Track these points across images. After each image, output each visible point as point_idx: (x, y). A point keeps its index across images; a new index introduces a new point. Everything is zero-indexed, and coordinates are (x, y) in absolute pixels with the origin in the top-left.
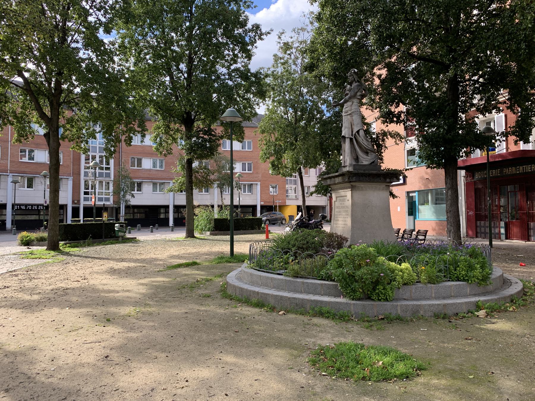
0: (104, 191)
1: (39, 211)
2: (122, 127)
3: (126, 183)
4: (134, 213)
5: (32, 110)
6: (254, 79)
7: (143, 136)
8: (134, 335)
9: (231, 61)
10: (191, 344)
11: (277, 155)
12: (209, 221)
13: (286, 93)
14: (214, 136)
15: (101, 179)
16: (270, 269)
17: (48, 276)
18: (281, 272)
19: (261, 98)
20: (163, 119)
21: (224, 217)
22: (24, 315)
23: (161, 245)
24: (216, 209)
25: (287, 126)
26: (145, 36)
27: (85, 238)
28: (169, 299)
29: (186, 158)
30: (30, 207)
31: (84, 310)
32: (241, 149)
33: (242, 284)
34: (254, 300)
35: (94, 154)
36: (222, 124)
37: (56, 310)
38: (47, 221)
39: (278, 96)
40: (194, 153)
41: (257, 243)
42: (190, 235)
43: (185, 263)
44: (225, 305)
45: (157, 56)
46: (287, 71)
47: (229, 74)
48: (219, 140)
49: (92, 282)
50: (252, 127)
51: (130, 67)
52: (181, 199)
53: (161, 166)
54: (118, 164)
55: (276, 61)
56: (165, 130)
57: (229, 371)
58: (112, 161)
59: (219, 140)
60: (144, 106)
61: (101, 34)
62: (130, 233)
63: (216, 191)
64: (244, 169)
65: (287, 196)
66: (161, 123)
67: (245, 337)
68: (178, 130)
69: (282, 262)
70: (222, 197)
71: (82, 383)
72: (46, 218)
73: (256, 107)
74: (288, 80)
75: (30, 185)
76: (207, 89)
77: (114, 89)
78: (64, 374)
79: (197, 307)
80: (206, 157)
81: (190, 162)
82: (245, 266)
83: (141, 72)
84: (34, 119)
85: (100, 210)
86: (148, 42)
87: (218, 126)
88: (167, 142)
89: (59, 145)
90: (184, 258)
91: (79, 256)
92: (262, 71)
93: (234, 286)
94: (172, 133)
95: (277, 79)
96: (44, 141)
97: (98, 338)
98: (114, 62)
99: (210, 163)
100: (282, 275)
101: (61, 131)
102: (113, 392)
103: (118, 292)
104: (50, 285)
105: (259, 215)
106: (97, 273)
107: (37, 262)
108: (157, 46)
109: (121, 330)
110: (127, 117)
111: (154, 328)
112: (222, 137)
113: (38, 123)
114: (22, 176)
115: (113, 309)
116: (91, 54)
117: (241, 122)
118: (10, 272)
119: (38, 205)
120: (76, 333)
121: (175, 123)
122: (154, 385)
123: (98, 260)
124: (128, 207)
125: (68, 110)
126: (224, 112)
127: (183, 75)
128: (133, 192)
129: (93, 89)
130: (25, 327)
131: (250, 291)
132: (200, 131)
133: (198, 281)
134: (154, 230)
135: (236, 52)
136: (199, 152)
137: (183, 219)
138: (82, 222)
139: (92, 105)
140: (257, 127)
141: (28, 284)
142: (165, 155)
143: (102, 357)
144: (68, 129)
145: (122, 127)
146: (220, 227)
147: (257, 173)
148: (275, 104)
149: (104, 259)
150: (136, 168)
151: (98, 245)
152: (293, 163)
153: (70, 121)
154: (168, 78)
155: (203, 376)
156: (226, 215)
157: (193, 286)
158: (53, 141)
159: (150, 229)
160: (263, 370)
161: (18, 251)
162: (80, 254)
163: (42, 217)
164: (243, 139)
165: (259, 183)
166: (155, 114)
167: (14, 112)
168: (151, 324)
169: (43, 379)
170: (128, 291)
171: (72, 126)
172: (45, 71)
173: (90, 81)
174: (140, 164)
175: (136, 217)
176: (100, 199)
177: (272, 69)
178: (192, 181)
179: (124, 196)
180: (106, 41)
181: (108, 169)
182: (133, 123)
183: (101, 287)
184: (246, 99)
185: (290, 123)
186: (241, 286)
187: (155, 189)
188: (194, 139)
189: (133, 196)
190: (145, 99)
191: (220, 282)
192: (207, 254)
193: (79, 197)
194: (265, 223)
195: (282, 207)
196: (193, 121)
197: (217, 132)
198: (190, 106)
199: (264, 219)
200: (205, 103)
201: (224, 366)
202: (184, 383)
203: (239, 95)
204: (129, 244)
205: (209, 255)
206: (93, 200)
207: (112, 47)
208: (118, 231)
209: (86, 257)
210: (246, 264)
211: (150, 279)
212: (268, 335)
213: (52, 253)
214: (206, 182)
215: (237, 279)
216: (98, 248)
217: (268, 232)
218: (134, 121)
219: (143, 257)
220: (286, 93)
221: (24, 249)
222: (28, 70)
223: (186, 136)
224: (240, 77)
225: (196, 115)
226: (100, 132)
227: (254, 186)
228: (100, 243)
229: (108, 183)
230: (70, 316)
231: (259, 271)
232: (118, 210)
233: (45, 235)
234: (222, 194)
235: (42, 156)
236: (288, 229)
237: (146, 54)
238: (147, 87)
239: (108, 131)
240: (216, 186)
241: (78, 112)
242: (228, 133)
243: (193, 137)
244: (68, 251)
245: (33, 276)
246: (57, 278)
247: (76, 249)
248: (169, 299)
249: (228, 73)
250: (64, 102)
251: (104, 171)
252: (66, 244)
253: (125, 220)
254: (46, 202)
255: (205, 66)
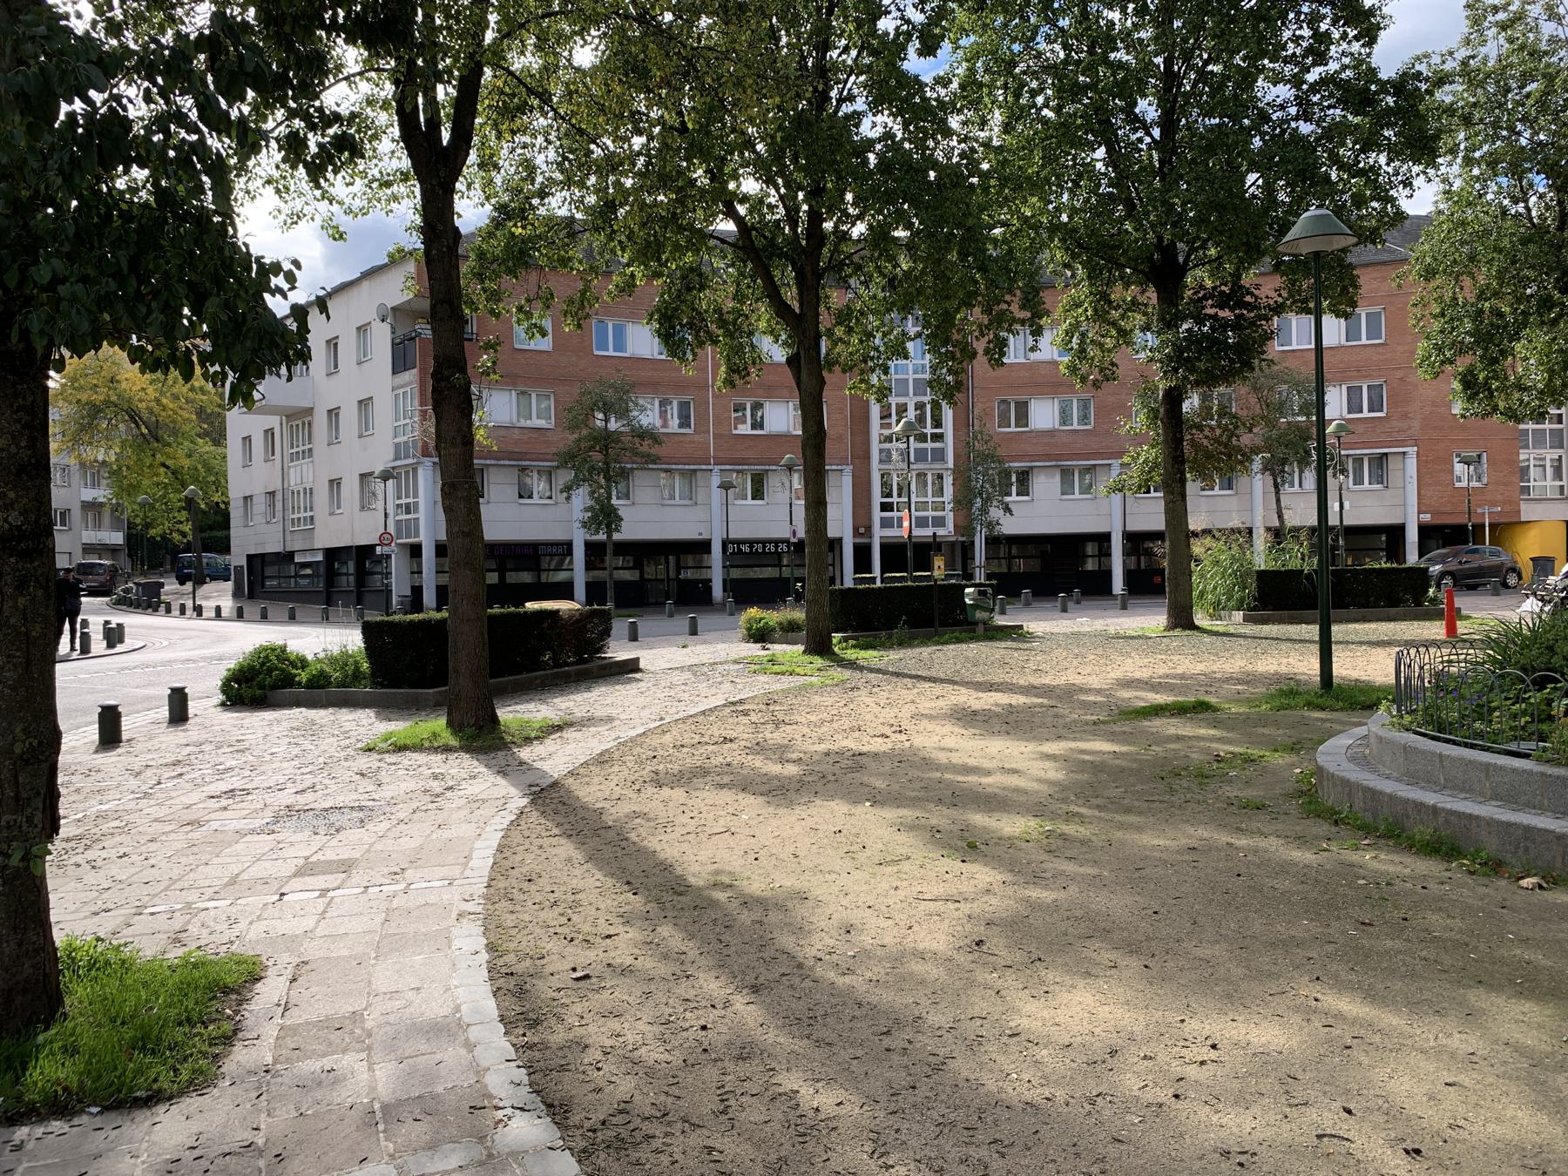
0: (930, 499)
1: (779, 555)
2: (977, 314)
3: (988, 473)
4: (1010, 558)
5: (757, 300)
6: (1390, 100)
7: (1037, 332)
8: (1047, 896)
9: (1304, 57)
10: (1217, 942)
11: (1486, 349)
12: (1242, 577)
13: (1519, 127)
14: (1251, 307)
15: (921, 466)
16: (1480, 735)
17: (813, 718)
18: (1524, 746)
19: (1417, 161)
20: (1089, 277)
21: (1295, 564)
22: (771, 809)
23: (1100, 650)
24: (1261, 541)
25: (1525, 241)
26: (1029, 41)
27: (890, 625)
28: (1137, 804)
29: (1162, 386)
30: (745, 548)
31: (908, 813)
32: (1343, 342)
33: (1372, 777)
34: (1423, 831)
35: (902, 400)
36: (1278, 267)
37: (839, 807)
38: (802, 580)
39: (1485, 141)
40: (1187, 369)
41: (1413, 651)
42: (1182, 619)
43: (1175, 703)
44: (1317, 838)
45: (1068, 91)
46: (1522, 48)
47: (1301, 101)
48: (1268, 319)
49: (919, 741)
50: (1384, 263)
51: (991, 139)
52: (1150, 514)
53: (1084, 418)
54: (962, 423)
55: (1476, 22)
56: (1095, 310)
57: (1349, 1042)
58: (948, 414)
59: (1268, 319)
60: (1036, 249)
61: (913, 63)
62: (1003, 612)
63: (1258, 483)
64: (1354, 406)
65: (1526, 490)
66: (1083, 291)
67: (1398, 944)
68: (1134, 305)
69: (1524, 713)
70: (1278, 501)
71: (924, 1002)
72: (798, 573)
73: (1400, 194)
74: (1526, 77)
75: (758, 494)
76: (1228, 162)
77: (955, 209)
78: (878, 971)
79: (1224, 838)
80: (1228, 377)
81: (1174, 398)
82: (1380, 722)
83: (1024, 148)
84: (762, 325)
85: (923, 552)
86: (1039, 55)
87: (1261, 274)
88: (1101, 345)
89: (823, 382)
90: (1170, 688)
91: (879, 671)
92: (1421, 67)
93: (1346, 783)
94: (1115, 314)
95: (1482, 84)
96: (788, 376)
97: (951, 889)
98: (948, 133)
99: (1237, 396)
100: (1526, 756)
101: (824, 344)
102: (1004, 1039)
103: (989, 773)
104: (821, 740)
105: (1412, 558)
106: (930, 717)
107: (787, 682)
108: (1066, 62)
109: (1009, 877)
110: (992, 283)
111: (1096, 882)
112: (1278, 309)
113: (771, 333)
114: (738, 472)
115: (978, 819)
116: (889, 121)
117: (1344, 250)
118: (733, 703)
119: (776, 542)
120: (895, 869)
121: (1127, 286)
122: (1117, 1042)
123: (927, 685)
124: (994, 541)
125: (838, 287)
126: (1285, 228)
127: (1149, 134)
128: (1007, 499)
129: (902, 219)
130: (778, 841)
131: (1406, 801)
132: (1205, 298)
133: (1218, 759)
134: (1070, 605)
135: (1323, 27)
136: (1201, 365)
137: (1154, 573)
138: (878, 584)
139: (896, 265)
140: (1404, 261)
141: (774, 737)
142: (1096, 385)
143: (967, 941)
144: (840, 339)
145: (977, 314)
146: (1276, 596)
147: (1405, 416)
148: (1476, 171)
149: (942, 681)
150: (1013, 429)
151: (924, 644)
152: (1551, 372)
153: (844, 316)
154: (1101, 152)
155: (1263, 1040)
156: (1298, 558)
157: (1206, 773)
158: (808, 373)
159: (1059, 604)
160: (1474, 1059)
161: (743, 654)
162: (882, 665)
163: (786, 572)
164: (1354, 305)
165: (1412, 450)
166: (1066, 266)
167: (719, 311)
168: (1090, 870)
169: (831, 975)
170: (1015, 771)
171: (850, 330)
172: (783, 191)
173: (889, 198)
174: (1022, 417)
175: (1015, 569)
176: (922, 522)
177: (1461, 54)
178: (1184, 457)
179: (984, 510)
180: (927, 79)
181: (938, 437)
182: (1008, 298)
183: (943, 757)
184: (1362, 173)
185: (1539, 230)
186: (1372, 784)
187: (1067, 488)
188: (1185, 326)
189: (1007, 509)
190: (1037, 227)
191: (1294, 766)
192: (1239, 681)
193: (870, 519)
194: (1438, 586)
195: (1504, 529)
196: (1183, 271)
197: (1261, 293)
198: (1174, 225)
199: (1436, 569)
200: (1224, 207)
201: (1330, 1021)
202: (1206, 1049)
203: (1335, 160)
204: (1003, 644)
205: (1248, 683)
206: (906, 524)
207: (943, 92)
208: (975, 607)
209: (898, 675)
210: (1383, 713)
211: (1073, 745)
212: (1482, 946)
213: (819, 661)
214: (1229, 456)
215: (1352, 759)
216: (925, 652)
217: (1452, 618)
218: (1011, 292)
219: (1047, 680)
220: (1519, 127)
221: (754, 649)
222: (744, 199)
223: (1162, 319)
224: (1343, 102)
225: (1193, 250)
226: (919, 335)
227: (1393, 464)
228: (929, 639)
229: (940, 477)
230: (876, 825)
231: (1434, 738)
232: (967, 549)
233: (799, 615)
234: (1277, 492)
235: (783, 418)
236: (1531, 605)
237: (1034, 93)
238: (1037, 186)
239: (940, 335)
240: (1257, 465)
241: (862, 290)
242: (1299, 292)
243: (1184, 319)
244: (854, 657)
245: (781, 716)
246: (835, 725)
247: (870, 653)
248: (1137, 804)
249: (1297, 97)
250: (829, 268)
251: (929, 445)
252: (846, 640)
253: (989, 577)
254: (794, 533)
255: (1218, 88)
